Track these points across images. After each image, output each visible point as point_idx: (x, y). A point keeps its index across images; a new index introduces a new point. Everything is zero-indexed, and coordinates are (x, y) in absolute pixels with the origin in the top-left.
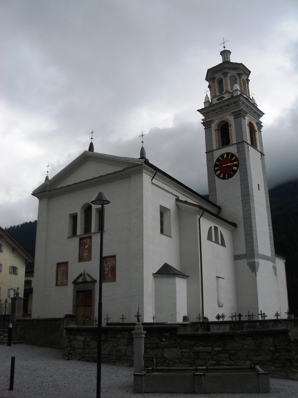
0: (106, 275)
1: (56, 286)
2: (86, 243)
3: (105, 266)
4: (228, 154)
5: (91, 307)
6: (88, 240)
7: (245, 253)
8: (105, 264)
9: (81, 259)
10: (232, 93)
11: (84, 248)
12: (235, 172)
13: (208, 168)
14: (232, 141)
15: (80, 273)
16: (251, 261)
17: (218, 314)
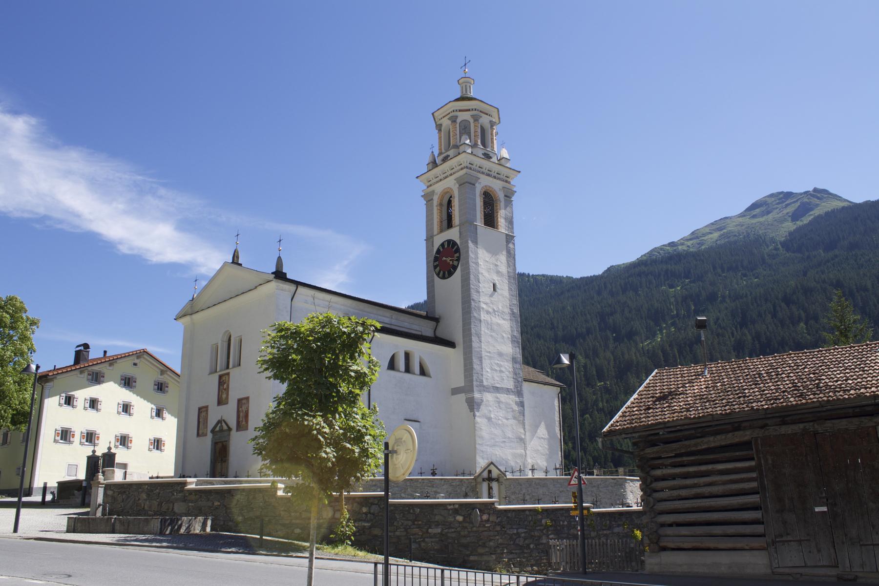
0: (241, 422)
4: (449, 241)
6: (227, 377)
7: (463, 385)
9: (220, 402)
13: (428, 263)
16: (469, 396)
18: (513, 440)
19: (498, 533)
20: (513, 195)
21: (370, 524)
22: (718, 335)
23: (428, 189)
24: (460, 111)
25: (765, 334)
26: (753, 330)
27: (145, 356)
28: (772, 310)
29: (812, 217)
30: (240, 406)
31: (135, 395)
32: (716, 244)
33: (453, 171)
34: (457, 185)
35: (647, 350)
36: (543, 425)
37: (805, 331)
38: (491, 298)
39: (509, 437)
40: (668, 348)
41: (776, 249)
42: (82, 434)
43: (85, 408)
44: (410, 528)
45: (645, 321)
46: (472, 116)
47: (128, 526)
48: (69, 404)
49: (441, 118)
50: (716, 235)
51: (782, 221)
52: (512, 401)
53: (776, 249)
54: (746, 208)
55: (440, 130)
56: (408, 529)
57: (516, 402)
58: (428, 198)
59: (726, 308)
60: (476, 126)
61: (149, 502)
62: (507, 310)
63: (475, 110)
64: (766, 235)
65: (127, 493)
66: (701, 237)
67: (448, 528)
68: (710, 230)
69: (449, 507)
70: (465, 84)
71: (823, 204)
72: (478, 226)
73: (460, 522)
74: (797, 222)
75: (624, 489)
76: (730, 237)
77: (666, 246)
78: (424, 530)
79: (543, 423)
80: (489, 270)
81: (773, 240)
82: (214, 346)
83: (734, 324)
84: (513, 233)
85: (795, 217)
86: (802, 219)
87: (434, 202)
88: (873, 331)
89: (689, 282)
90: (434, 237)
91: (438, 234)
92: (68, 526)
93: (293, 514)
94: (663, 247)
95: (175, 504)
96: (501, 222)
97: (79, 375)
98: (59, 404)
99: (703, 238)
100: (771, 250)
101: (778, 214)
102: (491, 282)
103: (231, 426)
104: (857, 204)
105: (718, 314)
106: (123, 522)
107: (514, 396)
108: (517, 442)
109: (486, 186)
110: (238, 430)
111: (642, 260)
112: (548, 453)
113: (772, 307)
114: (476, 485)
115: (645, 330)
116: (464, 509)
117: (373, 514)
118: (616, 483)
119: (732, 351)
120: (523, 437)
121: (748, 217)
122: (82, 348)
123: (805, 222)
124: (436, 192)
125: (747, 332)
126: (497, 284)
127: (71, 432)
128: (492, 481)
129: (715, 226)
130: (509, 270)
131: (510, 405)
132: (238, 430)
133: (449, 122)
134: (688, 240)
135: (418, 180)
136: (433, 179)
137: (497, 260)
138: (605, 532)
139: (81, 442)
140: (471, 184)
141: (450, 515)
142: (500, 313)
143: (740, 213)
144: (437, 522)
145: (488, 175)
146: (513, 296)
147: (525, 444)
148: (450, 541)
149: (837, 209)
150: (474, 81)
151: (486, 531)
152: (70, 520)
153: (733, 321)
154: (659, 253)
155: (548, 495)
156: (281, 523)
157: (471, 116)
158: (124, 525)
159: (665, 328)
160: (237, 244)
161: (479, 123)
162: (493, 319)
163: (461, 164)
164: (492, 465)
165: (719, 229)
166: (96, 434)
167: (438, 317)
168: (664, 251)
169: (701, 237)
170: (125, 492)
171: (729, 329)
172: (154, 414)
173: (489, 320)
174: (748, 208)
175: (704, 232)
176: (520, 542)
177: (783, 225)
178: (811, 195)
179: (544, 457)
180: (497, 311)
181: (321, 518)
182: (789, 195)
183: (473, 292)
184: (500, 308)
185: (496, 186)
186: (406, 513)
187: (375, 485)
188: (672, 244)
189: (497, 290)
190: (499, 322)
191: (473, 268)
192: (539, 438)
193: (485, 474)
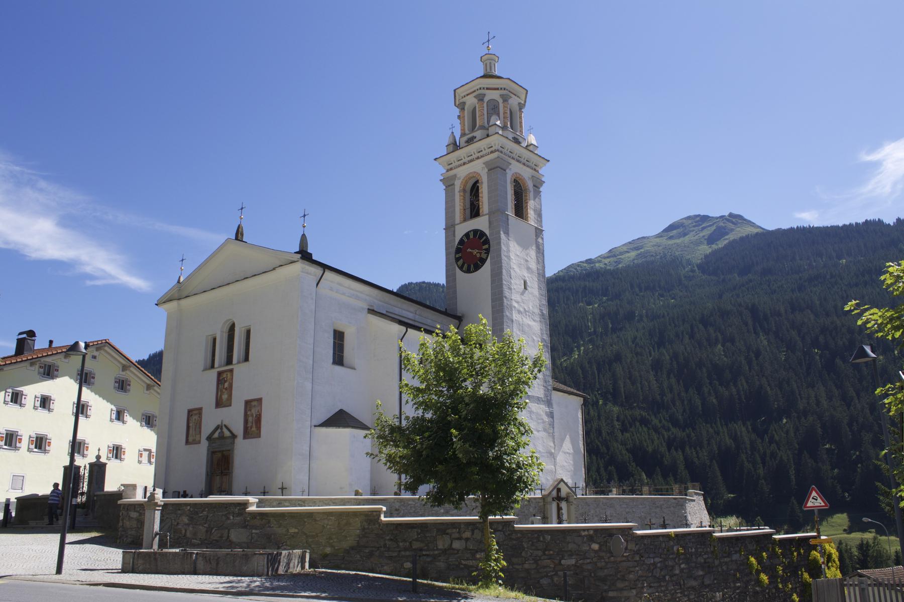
0: (249, 428)
1: (186, 445)
4: (475, 231)
9: (219, 404)
10: (488, 129)
11: (224, 387)
12: (483, 261)
13: (447, 254)
14: (483, 211)
15: (216, 425)
18: (543, 454)
19: (638, 564)
20: (542, 185)
22: (637, 354)
23: (448, 173)
24: (487, 89)
25: (683, 354)
26: (671, 351)
27: (106, 348)
28: (690, 331)
29: (727, 241)
30: (248, 409)
31: (93, 393)
32: (634, 263)
33: (481, 154)
34: (486, 170)
35: (566, 367)
36: (568, 438)
37: (722, 353)
39: (540, 451)
40: (587, 366)
41: (693, 271)
42: (31, 439)
43: (35, 408)
44: (540, 560)
45: (563, 336)
46: (502, 96)
47: (217, 564)
48: (16, 402)
49: (465, 96)
50: (633, 254)
51: (698, 243)
52: (543, 411)
53: (693, 271)
54: (664, 229)
55: (463, 109)
56: (538, 560)
57: (546, 412)
58: (448, 183)
59: (644, 328)
60: (506, 107)
61: (193, 527)
62: (537, 311)
63: (505, 89)
64: (682, 257)
66: (618, 255)
67: (583, 559)
68: (628, 249)
69: (583, 534)
70: (491, 61)
71: (738, 229)
72: (509, 216)
73: (596, 552)
74: (712, 246)
75: (685, 509)
77: (584, 263)
78: (557, 562)
79: (568, 436)
80: (520, 265)
81: (689, 262)
82: (210, 337)
83: (652, 344)
84: (542, 227)
85: (711, 240)
86: (717, 242)
87: (456, 187)
88: (785, 355)
89: (607, 299)
90: (456, 226)
91: (460, 223)
92: (124, 563)
93: (401, 544)
94: (580, 263)
95: (232, 531)
96: (531, 213)
97: (29, 368)
98: (5, 401)
99: (621, 257)
100: (687, 271)
101: (694, 236)
102: (522, 279)
103: (235, 432)
104: (770, 231)
105: (636, 333)
106: (209, 560)
107: (544, 406)
108: (548, 457)
110: (245, 438)
111: (560, 276)
112: (573, 469)
113: (689, 328)
114: (544, 505)
115: (562, 346)
116: (600, 535)
118: (677, 504)
119: (650, 370)
120: (553, 451)
121: (666, 238)
122: (25, 336)
123: (720, 246)
124: (458, 176)
125: (665, 352)
127: (17, 435)
128: (562, 500)
129: (632, 245)
130: (539, 267)
131: (540, 415)
132: (245, 438)
133: (475, 101)
134: (605, 258)
135: (436, 163)
136: (455, 162)
137: (527, 255)
138: (726, 559)
139: (29, 448)
140: (502, 169)
141: (585, 543)
143: (657, 233)
144: (570, 551)
145: (518, 161)
147: (554, 459)
148: (586, 574)
149: (751, 235)
150: (498, 59)
151: (624, 561)
152: (127, 555)
153: (651, 341)
154: (576, 269)
155: (615, 516)
156: (387, 555)
157: (500, 95)
158: (211, 563)
159: (583, 345)
161: (508, 104)
162: (524, 319)
163: (492, 147)
164: (562, 483)
165: (637, 249)
166: (47, 439)
167: (460, 315)
168: (581, 267)
169: (618, 255)
171: (647, 349)
172: (114, 416)
173: (521, 320)
174: (665, 229)
175: (622, 250)
176: (657, 573)
177: (699, 248)
178: (726, 219)
179: (569, 473)
181: (435, 548)
182: (705, 218)
183: (505, 288)
184: (531, 308)
185: (526, 173)
186: (535, 541)
188: (589, 261)
189: (528, 288)
190: (530, 323)
191: (505, 262)
192: (565, 453)
193: (554, 493)
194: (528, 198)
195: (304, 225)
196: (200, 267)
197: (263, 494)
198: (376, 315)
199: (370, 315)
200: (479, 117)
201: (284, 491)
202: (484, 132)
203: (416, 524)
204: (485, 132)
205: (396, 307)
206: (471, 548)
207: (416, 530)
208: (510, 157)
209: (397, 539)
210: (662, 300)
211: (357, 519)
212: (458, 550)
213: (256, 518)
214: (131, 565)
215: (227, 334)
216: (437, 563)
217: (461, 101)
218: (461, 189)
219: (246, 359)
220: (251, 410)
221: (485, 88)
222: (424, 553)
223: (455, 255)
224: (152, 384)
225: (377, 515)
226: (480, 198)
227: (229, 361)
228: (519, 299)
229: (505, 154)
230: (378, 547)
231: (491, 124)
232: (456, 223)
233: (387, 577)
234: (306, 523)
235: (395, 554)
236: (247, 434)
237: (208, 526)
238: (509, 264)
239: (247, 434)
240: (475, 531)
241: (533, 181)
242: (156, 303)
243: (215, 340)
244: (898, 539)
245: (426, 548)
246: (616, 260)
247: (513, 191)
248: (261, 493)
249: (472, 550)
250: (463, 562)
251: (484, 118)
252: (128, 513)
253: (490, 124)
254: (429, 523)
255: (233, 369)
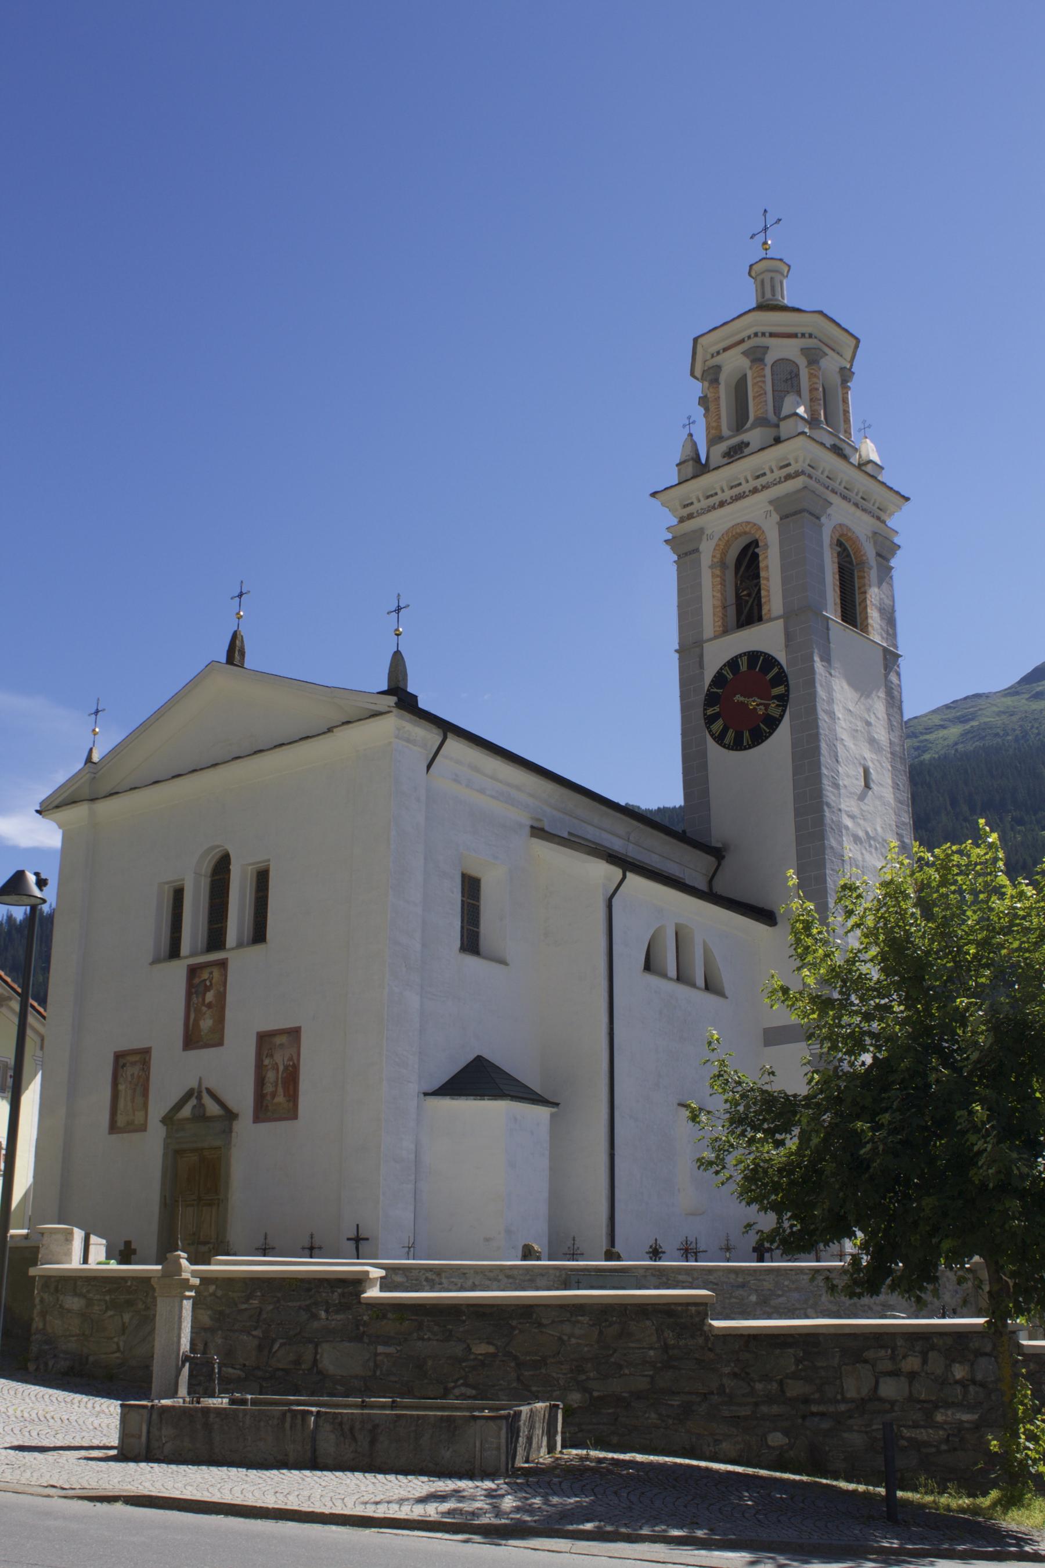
0: (269, 1098)
2: (208, 983)
3: (267, 1066)
4: (753, 656)
5: (218, 1205)
8: (266, 1057)
9: (192, 1040)
10: (777, 426)
11: (204, 999)
12: (773, 723)
13: (685, 708)
14: (769, 611)
15: (187, 1089)
17: (656, 1240)
21: (976, 1417)
24: (772, 335)
32: (956, 750)
33: (763, 481)
34: (776, 517)
38: (861, 803)
46: (805, 351)
47: (373, 1442)
49: (718, 353)
50: (954, 732)
54: (1022, 676)
60: (815, 376)
63: (810, 336)
65: (141, 1306)
66: (922, 733)
68: (942, 720)
70: (773, 275)
72: (830, 621)
76: (986, 736)
82: (166, 886)
87: (702, 556)
90: (706, 646)
91: (716, 637)
93: (759, 1386)
96: (874, 617)
99: (927, 737)
102: (860, 764)
106: (352, 1429)
109: (840, 525)
110: (257, 1119)
117: (982, 1385)
121: (1027, 696)
124: (708, 532)
126: (871, 771)
129: (953, 711)
130: (892, 739)
132: (257, 1119)
133: (745, 362)
135: (655, 502)
137: (868, 710)
140: (811, 514)
142: (879, 843)
145: (844, 498)
146: (902, 804)
156: (727, 1414)
157: (802, 349)
158: (354, 1439)
160: (240, 618)
161: (820, 369)
162: (867, 856)
163: (788, 465)
165: (962, 720)
167: (719, 845)
170: (130, 1303)
173: (860, 859)
180: (874, 839)
184: (879, 829)
185: (861, 526)
187: (743, 1286)
189: (872, 785)
194: (866, 581)
195: (397, 630)
196: (144, 728)
197: (307, 1252)
198: (551, 842)
199: (535, 840)
200: (754, 398)
201: (363, 1245)
202: (769, 433)
203: (791, 1335)
204: (771, 432)
205: (589, 824)
206: (923, 1397)
207: (791, 1351)
208: (827, 488)
209: (747, 1374)
210: (1019, 832)
211: (648, 1323)
212: (893, 1403)
213: (384, 1317)
214: (144, 1439)
215: (209, 880)
216: (846, 1435)
217: (712, 362)
218: (716, 560)
219: (259, 934)
220: (272, 1056)
221: (767, 335)
222: (814, 1408)
223: (705, 710)
224: (7, 994)
225: (698, 1313)
226: (763, 582)
227: (216, 940)
228: (856, 811)
229: (818, 481)
230: (705, 1394)
231: (785, 412)
232: (705, 637)
233: (739, 1469)
234: (517, 1332)
235: (745, 1411)
236: (263, 1111)
237: (261, 1335)
238: (833, 731)
239: (263, 1111)
240: (930, 1354)
241: (875, 543)
242: (38, 809)
243: (178, 894)
244: (104, 1242)
245: (817, 1396)
246: (918, 744)
247: (836, 566)
248: (303, 1248)
249: (924, 1402)
250: (906, 1433)
251: (766, 401)
252: (58, 1299)
253: (783, 415)
254: (823, 1334)
255: (227, 959)
